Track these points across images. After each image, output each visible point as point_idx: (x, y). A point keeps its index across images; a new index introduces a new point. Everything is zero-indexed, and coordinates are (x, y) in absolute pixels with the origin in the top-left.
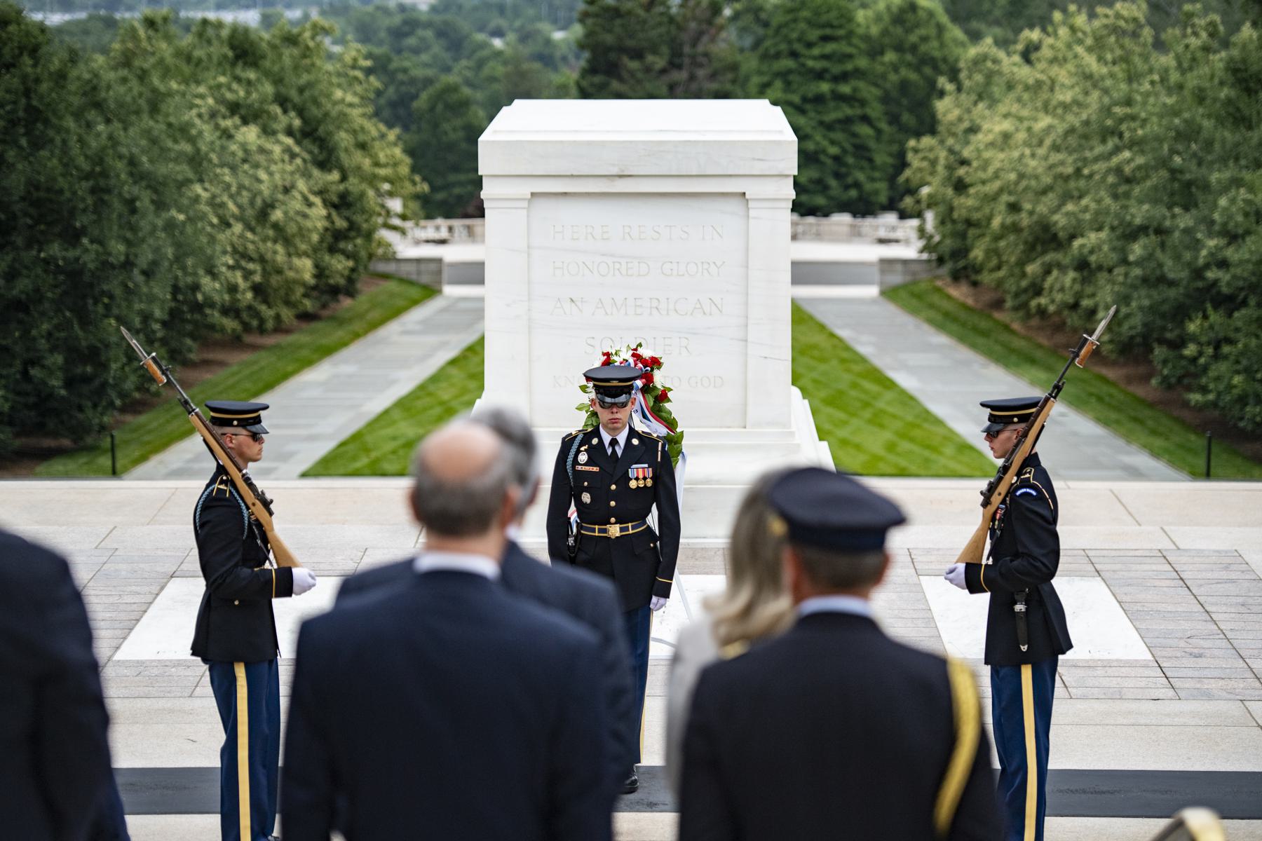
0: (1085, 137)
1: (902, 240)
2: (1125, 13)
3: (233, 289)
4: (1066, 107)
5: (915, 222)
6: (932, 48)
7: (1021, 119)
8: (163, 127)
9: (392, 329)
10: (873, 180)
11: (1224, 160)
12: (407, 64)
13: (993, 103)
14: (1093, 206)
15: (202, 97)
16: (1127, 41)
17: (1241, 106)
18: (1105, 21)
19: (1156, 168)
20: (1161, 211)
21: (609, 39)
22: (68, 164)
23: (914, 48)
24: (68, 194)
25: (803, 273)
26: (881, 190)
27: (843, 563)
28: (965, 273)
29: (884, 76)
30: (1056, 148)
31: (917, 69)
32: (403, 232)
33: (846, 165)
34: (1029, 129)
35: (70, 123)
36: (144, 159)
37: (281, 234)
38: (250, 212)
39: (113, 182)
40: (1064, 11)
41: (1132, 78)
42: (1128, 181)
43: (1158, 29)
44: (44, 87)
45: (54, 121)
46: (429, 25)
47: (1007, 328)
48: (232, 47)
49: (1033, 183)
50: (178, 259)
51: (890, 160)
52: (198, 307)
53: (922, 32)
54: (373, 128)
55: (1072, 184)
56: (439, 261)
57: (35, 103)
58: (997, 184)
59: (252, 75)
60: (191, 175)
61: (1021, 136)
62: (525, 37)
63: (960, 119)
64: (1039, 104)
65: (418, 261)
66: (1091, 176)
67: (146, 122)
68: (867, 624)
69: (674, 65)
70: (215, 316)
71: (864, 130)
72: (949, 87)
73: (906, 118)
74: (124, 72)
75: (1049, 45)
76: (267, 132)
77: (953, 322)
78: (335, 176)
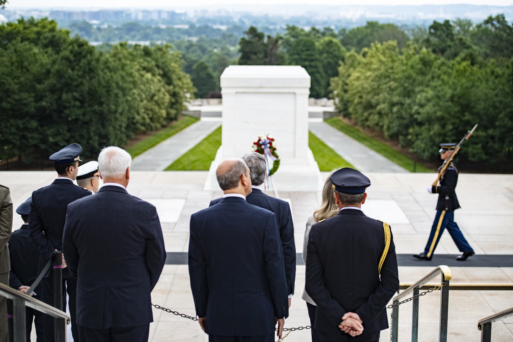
1: (329, 106)
3: (144, 119)
4: (375, 70)
5: (331, 102)
6: (336, 53)
9: (187, 130)
13: (355, 68)
16: (392, 52)
20: (401, 99)
21: (247, 49)
25: (219, 115)
26: (323, 92)
27: (349, 197)
28: (347, 115)
30: (372, 81)
32: (190, 103)
35: (100, 73)
37: (157, 103)
38: (149, 98)
41: (393, 61)
43: (400, 48)
46: (196, 45)
47: (358, 131)
50: (129, 111)
52: (134, 124)
54: (182, 74)
56: (199, 112)
58: (355, 91)
59: (149, 59)
61: (363, 77)
62: (223, 49)
67: (121, 72)
68: (360, 212)
69: (266, 56)
70: (139, 126)
73: (330, 72)
74: (114, 59)
75: (370, 52)
76: (154, 75)
77: (344, 129)
78: (171, 87)
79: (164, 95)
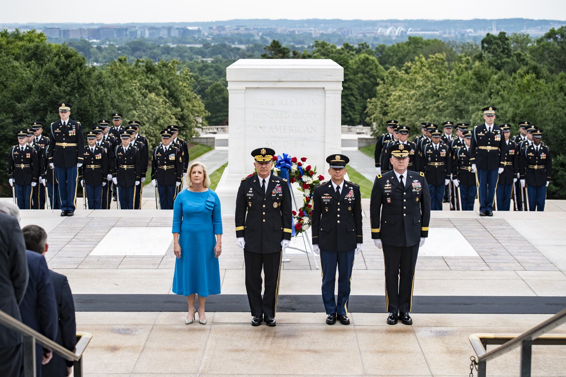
0: (426, 97)
2: (438, 57)
4: (419, 87)
6: (374, 72)
7: (405, 91)
8: (122, 91)
10: (355, 114)
11: (473, 103)
12: (204, 79)
14: (429, 118)
15: (136, 83)
17: (478, 86)
18: (432, 59)
19: (451, 106)
22: (91, 101)
23: (368, 72)
24: (91, 112)
26: (357, 117)
29: (358, 81)
31: (369, 79)
33: (346, 110)
34: (408, 94)
36: (116, 101)
39: (106, 108)
40: (419, 56)
42: (440, 111)
44: (84, 77)
45: (86, 88)
46: (212, 67)
48: (146, 68)
49: (409, 111)
51: (360, 108)
53: (371, 67)
54: (193, 95)
55: (422, 112)
56: (214, 138)
57: (81, 82)
58: (397, 113)
60: (132, 107)
63: (385, 92)
64: (411, 86)
65: (207, 138)
66: (428, 109)
71: (352, 98)
72: (381, 82)
76: (158, 95)
78: (179, 109)
79: (171, 118)
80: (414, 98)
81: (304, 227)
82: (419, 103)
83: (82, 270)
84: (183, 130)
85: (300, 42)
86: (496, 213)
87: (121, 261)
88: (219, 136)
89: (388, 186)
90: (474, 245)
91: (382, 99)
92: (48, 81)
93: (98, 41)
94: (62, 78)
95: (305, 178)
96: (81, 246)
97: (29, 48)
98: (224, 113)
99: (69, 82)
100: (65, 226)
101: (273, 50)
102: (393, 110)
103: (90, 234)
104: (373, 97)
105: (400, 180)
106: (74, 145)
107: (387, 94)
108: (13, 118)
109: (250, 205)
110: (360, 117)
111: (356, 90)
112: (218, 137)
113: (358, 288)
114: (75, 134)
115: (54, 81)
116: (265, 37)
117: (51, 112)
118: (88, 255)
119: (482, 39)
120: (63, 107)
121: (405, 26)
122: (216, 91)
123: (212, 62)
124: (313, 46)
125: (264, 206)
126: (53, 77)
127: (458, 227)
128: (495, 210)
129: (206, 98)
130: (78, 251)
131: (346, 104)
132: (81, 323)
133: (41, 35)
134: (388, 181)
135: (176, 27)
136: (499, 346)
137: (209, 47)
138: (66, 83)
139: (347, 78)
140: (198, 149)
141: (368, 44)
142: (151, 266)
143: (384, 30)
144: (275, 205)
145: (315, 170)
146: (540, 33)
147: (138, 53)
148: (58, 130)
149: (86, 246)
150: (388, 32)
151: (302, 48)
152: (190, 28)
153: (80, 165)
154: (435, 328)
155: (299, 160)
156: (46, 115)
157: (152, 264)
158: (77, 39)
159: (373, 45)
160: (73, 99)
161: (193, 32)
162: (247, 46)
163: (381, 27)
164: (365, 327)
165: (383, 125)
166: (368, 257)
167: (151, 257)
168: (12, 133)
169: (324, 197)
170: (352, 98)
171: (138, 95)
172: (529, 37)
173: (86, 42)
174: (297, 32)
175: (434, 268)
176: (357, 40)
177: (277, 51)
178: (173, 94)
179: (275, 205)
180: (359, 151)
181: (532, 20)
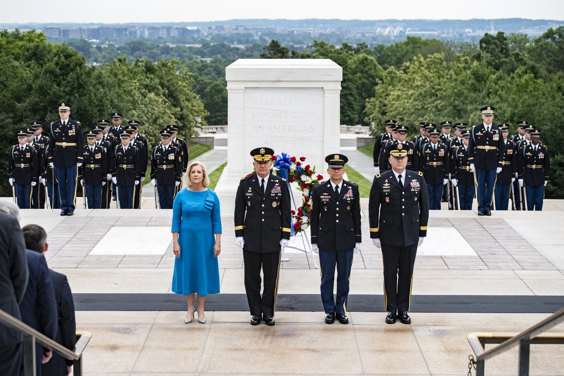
0: (425, 96)
2: (437, 57)
4: (417, 86)
6: (372, 72)
7: (404, 91)
8: (122, 91)
10: (353, 114)
11: (471, 103)
12: (203, 78)
13: (394, 86)
14: (428, 118)
15: (135, 83)
17: (476, 85)
18: (431, 59)
19: (449, 106)
22: (90, 101)
23: (367, 72)
24: (90, 112)
26: (356, 117)
31: (368, 79)
33: (345, 109)
34: (406, 94)
36: (116, 101)
39: (105, 108)
40: (417, 56)
42: (439, 110)
44: (84, 76)
45: (86, 87)
46: (211, 67)
48: (146, 67)
49: (408, 111)
51: (359, 108)
53: (369, 67)
54: (192, 94)
55: (421, 112)
56: (213, 138)
57: (80, 82)
58: (395, 112)
60: (131, 107)
63: (383, 92)
64: (409, 86)
65: (206, 138)
66: (427, 109)
71: (351, 98)
72: (380, 82)
76: (157, 94)
78: (178, 109)
79: (171, 118)
80: (413, 98)
81: (303, 227)
82: (417, 103)
83: (82, 270)
84: (182, 129)
85: (299, 42)
86: (494, 212)
87: (121, 261)
88: (218, 136)
89: (386, 185)
90: (472, 244)
91: (380, 99)
92: (48, 81)
93: (98, 41)
94: (61, 78)
95: (304, 178)
96: (81, 245)
97: (29, 48)
98: (224, 113)
99: (69, 82)
100: (64, 225)
101: (272, 50)
102: (392, 109)
103: (90, 234)
104: (372, 97)
105: (398, 180)
106: (73, 144)
107: (386, 93)
108: (13, 118)
109: (249, 205)
110: (359, 117)
111: (354, 90)
112: (217, 136)
113: (357, 287)
114: (74, 134)
115: (54, 81)
116: (264, 37)
117: (51, 112)
118: (87, 254)
119: (480, 38)
120: (63, 107)
121: (404, 26)
122: (216, 91)
123: (212, 62)
124: (312, 46)
125: (263, 205)
126: (53, 77)
127: (456, 227)
128: (493, 209)
129: (205, 98)
130: (78, 251)
131: (345, 103)
132: (81, 322)
133: (41, 35)
134: (387, 181)
135: (176, 27)
136: (497, 345)
137: (208, 47)
138: (66, 82)
139: (346, 78)
140: (198, 149)
141: (366, 44)
142: (150, 266)
143: (382, 30)
144: (274, 205)
145: (314, 170)
146: (538, 33)
147: (138, 52)
148: (58, 130)
149: (86, 245)
150: (386, 32)
151: (301, 48)
152: (189, 28)
153: (79, 165)
154: (433, 327)
155: (298, 160)
156: (45, 114)
157: (152, 264)
158: (77, 39)
159: (371, 45)
160: (72, 98)
161: (192, 32)
162: (246, 45)
163: (380, 26)
164: (363, 326)
165: (381, 125)
166: (366, 256)
167: (150, 256)
168: (12, 133)
169: (323, 197)
170: (351, 98)
171: (137, 94)
172: (527, 37)
173: (85, 41)
174: (295, 32)
175: (433, 268)
176: (356, 40)
177: (276, 51)
178: (173, 94)
179: (274, 205)
180: (357, 151)
181: (530, 20)
